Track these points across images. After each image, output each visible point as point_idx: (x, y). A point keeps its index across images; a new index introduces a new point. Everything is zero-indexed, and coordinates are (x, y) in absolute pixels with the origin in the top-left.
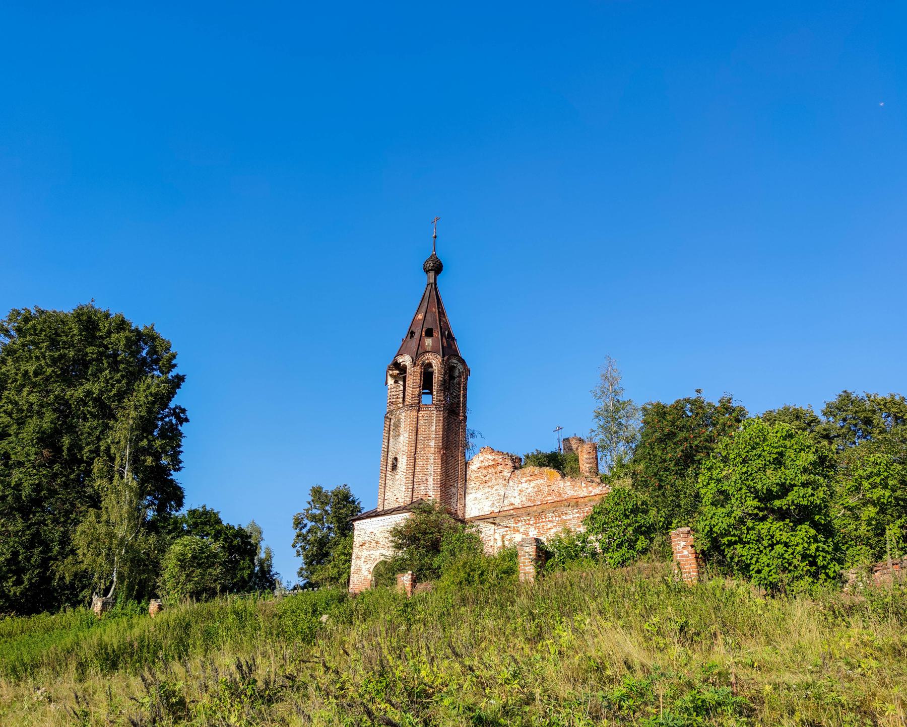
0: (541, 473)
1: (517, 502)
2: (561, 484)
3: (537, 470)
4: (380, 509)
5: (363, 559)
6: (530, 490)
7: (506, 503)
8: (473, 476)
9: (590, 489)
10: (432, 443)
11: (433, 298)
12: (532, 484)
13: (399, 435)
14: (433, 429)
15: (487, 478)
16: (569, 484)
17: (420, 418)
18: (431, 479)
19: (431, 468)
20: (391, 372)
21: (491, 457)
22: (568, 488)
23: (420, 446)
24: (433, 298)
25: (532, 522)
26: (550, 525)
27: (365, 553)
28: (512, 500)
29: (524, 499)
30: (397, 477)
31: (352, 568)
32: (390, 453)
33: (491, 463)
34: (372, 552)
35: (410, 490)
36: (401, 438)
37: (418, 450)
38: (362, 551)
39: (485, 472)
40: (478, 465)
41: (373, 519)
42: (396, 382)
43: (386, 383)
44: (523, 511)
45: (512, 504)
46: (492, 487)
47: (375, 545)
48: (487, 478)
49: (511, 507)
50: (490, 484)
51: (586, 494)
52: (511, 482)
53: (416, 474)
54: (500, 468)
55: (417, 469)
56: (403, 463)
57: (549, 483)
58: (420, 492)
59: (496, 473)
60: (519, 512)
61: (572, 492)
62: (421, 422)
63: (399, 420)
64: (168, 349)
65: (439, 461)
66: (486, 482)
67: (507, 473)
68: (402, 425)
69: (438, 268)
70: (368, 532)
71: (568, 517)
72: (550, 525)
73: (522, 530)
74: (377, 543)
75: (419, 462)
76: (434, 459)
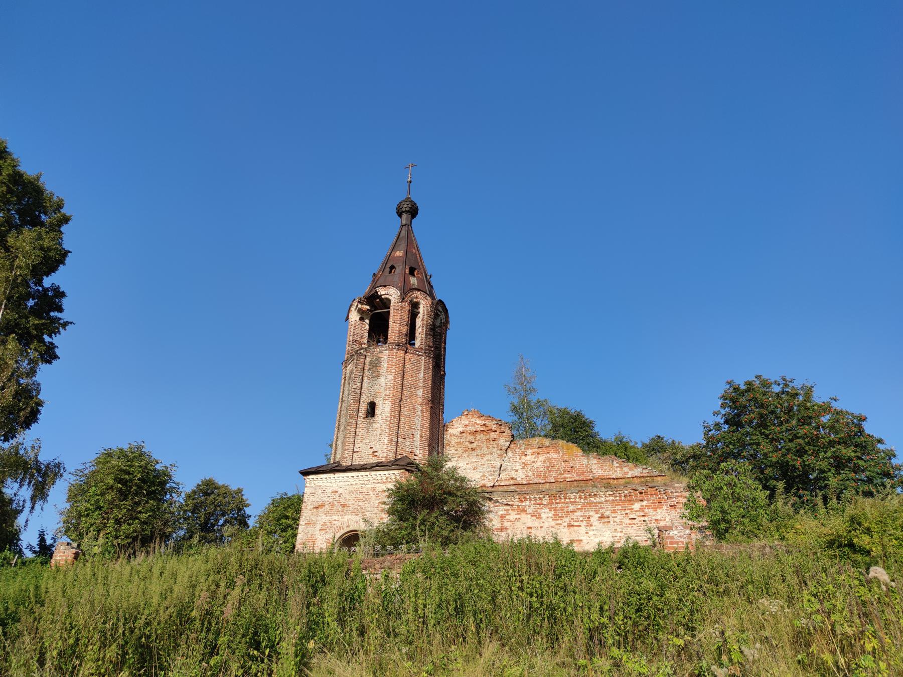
0: (553, 446)
1: (520, 477)
2: (584, 461)
3: (548, 442)
4: (346, 463)
5: (318, 527)
6: (539, 464)
7: (503, 475)
8: (453, 442)
9: (626, 469)
10: (420, 392)
11: (407, 239)
12: (541, 458)
13: (378, 376)
14: (421, 376)
15: (474, 446)
16: (595, 461)
17: (407, 361)
18: (417, 435)
19: (418, 422)
20: (360, 306)
21: (478, 421)
22: (594, 466)
23: (406, 393)
24: (407, 239)
25: (545, 502)
26: (571, 508)
27: (322, 518)
28: (513, 474)
29: (530, 474)
30: (375, 426)
31: (299, 537)
32: (363, 398)
33: (480, 428)
34: (336, 517)
35: (394, 443)
36: (382, 380)
37: (404, 398)
38: (317, 515)
39: (472, 438)
40: (461, 429)
41: (337, 475)
42: (362, 319)
43: (347, 319)
44: (530, 488)
45: (513, 479)
46: (483, 456)
47: (340, 508)
48: (474, 446)
49: (512, 482)
50: (479, 452)
51: (620, 476)
52: (509, 452)
53: (401, 426)
54: (493, 435)
55: (403, 420)
56: (384, 409)
57: (566, 458)
58: (406, 449)
59: (487, 440)
60: (524, 489)
61: (600, 472)
62: (407, 366)
63: (378, 359)
64: (59, 207)
65: (428, 415)
66: (473, 449)
67: (504, 442)
68: (385, 365)
69: (413, 212)
70: (329, 491)
71: (598, 500)
72: (571, 508)
73: (529, 511)
74: (343, 506)
75: (405, 412)
76: (422, 411)
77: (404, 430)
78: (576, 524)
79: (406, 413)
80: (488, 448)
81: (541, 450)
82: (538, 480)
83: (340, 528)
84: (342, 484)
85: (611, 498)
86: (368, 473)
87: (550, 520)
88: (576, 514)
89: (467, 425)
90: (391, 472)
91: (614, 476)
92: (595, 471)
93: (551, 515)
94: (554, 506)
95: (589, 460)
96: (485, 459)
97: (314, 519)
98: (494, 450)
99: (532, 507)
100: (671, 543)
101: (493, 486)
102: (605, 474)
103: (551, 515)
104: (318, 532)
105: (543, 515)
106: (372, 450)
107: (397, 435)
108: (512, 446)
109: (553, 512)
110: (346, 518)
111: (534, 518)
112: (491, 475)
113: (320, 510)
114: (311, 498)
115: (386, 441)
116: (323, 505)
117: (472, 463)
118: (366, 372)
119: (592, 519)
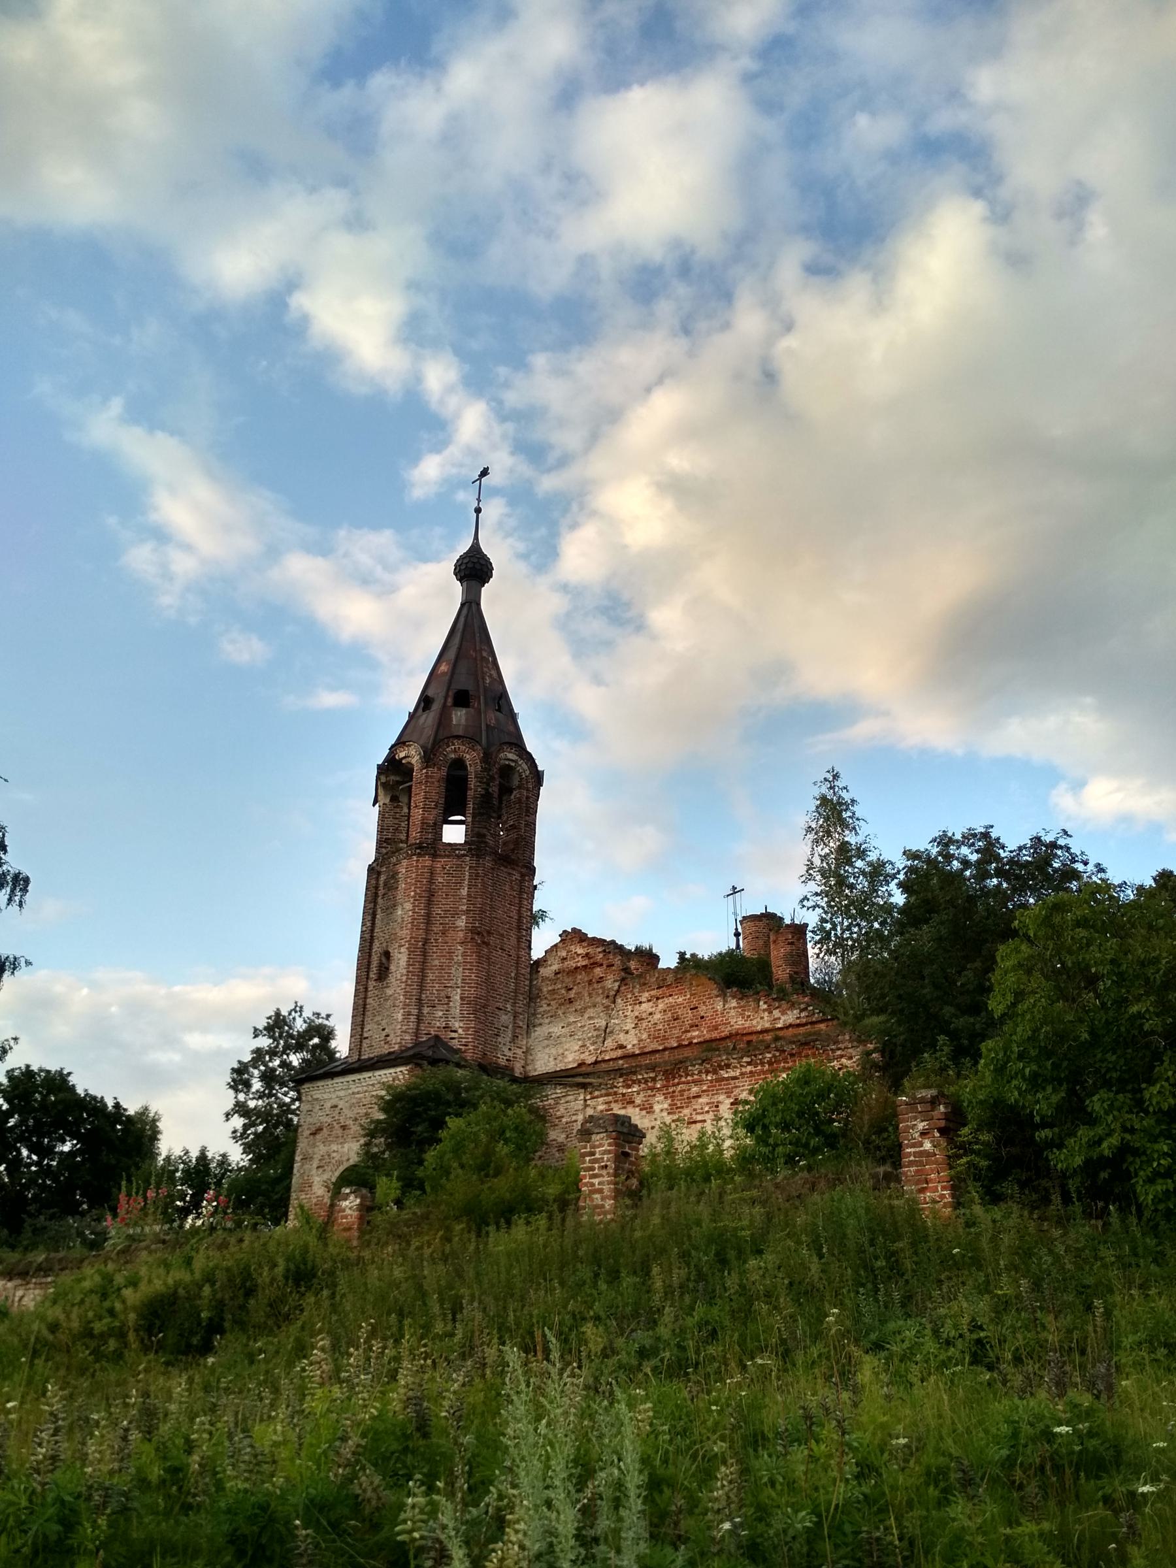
1: (631, 1042)
6: (658, 1016)
9: (776, 1013)
12: (661, 1006)
15: (572, 994)
19: (458, 973)
22: (733, 1013)
23: (436, 928)
26: (695, 1089)
28: (622, 1039)
30: (389, 992)
32: (376, 944)
34: (334, 1147)
35: (413, 1018)
38: (314, 1146)
39: (568, 981)
40: (555, 967)
41: (337, 1080)
46: (582, 1012)
47: (340, 1132)
48: (572, 994)
49: (619, 1053)
50: (578, 1005)
52: (619, 1001)
59: (590, 982)
66: (571, 1001)
71: (732, 1074)
72: (695, 1089)
73: (638, 1101)
76: (464, 955)
77: (433, 989)
78: (699, 1118)
79: (436, 962)
80: (590, 995)
81: (660, 991)
82: (655, 1046)
83: (340, 1163)
84: (342, 1093)
85: (749, 1068)
86: (370, 1074)
87: (665, 1114)
88: (701, 1100)
89: (564, 959)
90: (399, 1069)
91: (759, 1028)
92: (733, 1021)
93: (666, 1106)
94: (671, 1090)
95: (725, 1002)
96: (586, 1016)
97: (310, 1151)
98: (599, 999)
99: (642, 1094)
100: (343, 1217)
101: (596, 1062)
102: (747, 1024)
103: (666, 1106)
104: (314, 1172)
105: (657, 1108)
106: (384, 1033)
107: (419, 1001)
108: (623, 988)
109: (669, 1101)
110: (346, 1146)
111: (644, 1112)
112: (593, 1044)
113: (318, 1137)
114: (309, 1119)
115: (400, 1017)
116: (320, 1129)
117: (569, 1024)
118: (380, 900)
119: (721, 1107)
